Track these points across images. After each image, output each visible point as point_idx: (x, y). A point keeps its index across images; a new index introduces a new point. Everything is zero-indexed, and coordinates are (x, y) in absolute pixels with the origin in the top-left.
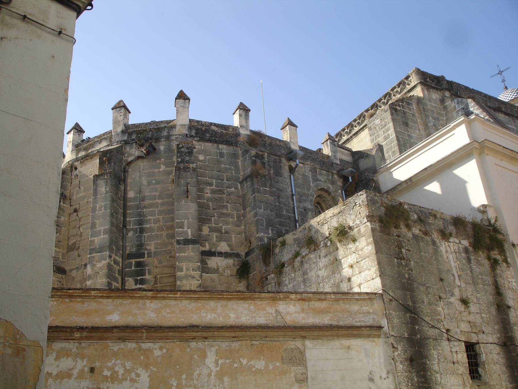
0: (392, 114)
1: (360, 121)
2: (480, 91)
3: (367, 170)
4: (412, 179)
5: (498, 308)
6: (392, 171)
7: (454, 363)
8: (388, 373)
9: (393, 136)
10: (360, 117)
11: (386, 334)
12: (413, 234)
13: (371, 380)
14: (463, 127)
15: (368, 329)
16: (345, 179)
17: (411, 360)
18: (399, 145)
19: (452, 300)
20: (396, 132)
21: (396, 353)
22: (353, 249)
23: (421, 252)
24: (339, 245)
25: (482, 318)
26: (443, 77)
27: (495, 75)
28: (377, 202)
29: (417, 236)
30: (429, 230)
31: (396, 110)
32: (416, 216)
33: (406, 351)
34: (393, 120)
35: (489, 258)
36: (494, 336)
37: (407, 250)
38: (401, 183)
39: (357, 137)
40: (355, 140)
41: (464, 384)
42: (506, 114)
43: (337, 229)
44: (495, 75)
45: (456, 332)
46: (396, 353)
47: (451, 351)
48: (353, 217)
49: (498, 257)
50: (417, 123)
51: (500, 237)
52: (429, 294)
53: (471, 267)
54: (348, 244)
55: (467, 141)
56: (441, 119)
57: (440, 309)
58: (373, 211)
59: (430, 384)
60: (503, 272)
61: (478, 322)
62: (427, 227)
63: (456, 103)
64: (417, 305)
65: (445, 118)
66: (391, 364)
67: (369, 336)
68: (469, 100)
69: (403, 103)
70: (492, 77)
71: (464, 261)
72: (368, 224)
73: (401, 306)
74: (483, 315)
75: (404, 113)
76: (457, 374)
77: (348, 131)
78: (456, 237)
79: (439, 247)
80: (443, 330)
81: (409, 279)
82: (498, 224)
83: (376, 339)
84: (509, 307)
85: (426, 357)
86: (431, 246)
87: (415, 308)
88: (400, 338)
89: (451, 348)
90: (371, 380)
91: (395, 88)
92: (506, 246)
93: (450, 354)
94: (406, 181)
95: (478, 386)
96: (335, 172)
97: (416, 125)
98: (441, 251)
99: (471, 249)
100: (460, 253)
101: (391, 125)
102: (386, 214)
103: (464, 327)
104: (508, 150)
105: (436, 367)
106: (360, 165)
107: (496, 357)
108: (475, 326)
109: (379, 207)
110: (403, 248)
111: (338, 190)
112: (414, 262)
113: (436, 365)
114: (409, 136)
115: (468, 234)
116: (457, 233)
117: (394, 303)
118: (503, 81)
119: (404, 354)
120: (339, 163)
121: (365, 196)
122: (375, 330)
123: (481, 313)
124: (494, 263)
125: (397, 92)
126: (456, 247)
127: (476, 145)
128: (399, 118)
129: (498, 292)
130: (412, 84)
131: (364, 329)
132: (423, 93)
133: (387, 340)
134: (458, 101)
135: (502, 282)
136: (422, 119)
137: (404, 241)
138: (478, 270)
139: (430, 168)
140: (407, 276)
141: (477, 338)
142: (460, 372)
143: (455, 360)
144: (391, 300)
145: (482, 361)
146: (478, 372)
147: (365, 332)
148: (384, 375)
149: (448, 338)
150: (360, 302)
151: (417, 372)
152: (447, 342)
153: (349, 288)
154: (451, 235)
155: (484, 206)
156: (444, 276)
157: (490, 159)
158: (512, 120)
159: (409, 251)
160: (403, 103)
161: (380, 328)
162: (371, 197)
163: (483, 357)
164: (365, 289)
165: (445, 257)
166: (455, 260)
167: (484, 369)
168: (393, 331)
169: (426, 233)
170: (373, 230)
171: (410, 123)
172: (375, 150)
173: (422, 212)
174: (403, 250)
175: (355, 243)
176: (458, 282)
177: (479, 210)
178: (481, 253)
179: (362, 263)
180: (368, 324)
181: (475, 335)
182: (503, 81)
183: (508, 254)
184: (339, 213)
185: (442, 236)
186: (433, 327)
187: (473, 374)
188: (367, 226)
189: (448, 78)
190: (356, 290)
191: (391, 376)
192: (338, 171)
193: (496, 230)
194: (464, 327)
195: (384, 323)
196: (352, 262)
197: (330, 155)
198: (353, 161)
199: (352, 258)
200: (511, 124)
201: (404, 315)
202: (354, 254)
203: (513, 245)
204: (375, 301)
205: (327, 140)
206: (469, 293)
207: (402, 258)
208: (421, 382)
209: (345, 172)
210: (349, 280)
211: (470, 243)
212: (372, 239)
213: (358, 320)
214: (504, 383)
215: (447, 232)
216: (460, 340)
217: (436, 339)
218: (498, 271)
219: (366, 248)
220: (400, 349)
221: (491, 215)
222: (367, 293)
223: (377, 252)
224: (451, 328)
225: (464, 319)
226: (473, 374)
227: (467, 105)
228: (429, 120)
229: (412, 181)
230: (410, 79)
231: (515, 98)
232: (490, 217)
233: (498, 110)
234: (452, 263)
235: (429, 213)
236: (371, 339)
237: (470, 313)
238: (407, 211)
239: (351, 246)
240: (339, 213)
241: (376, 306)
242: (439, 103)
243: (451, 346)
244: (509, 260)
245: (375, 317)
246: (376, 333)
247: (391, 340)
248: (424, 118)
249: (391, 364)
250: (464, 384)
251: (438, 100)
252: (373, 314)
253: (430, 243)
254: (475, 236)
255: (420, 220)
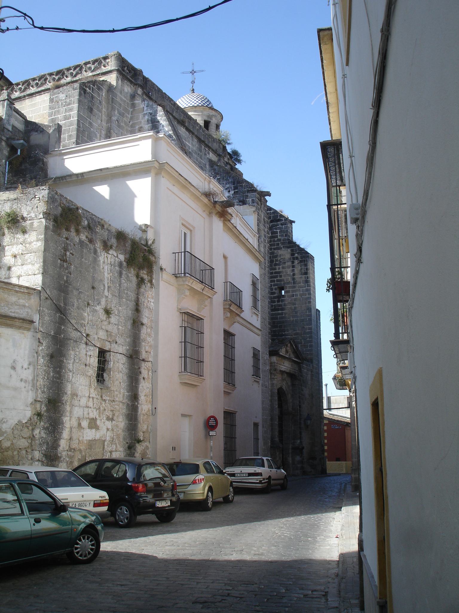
0: (80, 95)
1: (40, 83)
2: (171, 97)
3: (38, 146)
4: (84, 175)
5: (134, 323)
6: (65, 157)
7: (86, 365)
8: (30, 364)
9: (74, 119)
10: (40, 78)
11: (35, 329)
12: (80, 240)
13: (14, 368)
14: (149, 141)
15: (21, 321)
16: (13, 149)
17: (52, 356)
18: (79, 130)
19: (98, 308)
20: (79, 116)
21: (41, 348)
22: (21, 240)
23: (82, 258)
24: (6, 231)
25: (118, 329)
26: (141, 71)
27: (186, 73)
28: (56, 200)
29: (83, 242)
30: (94, 238)
31: (85, 91)
32: (86, 222)
33: (49, 347)
34: (80, 102)
35: (137, 276)
36: (124, 348)
37: (71, 253)
38: (72, 175)
39: (30, 99)
40: (27, 102)
41: (90, 385)
42: (187, 129)
43: (9, 215)
44: (186, 73)
45: (94, 338)
46: (41, 348)
47: (86, 354)
48: (29, 208)
49: (145, 277)
50: (102, 113)
51: (152, 258)
52: (80, 298)
53: (120, 281)
54: (17, 234)
55: (148, 157)
56: (126, 116)
57: (86, 314)
58: (50, 208)
59: (62, 380)
60: (146, 291)
61: (114, 332)
62: (93, 235)
63: (146, 105)
64: (67, 307)
65: (129, 116)
66: (34, 356)
67: (20, 328)
68: (160, 108)
69: (94, 86)
70: (183, 73)
71: (116, 275)
72: (43, 220)
73: (53, 305)
74: (120, 327)
75: (93, 97)
76: (87, 375)
77: (23, 88)
78: (115, 251)
79: (98, 256)
80: (84, 334)
81: (66, 282)
82: (153, 247)
83: (25, 332)
84: (142, 324)
85: (64, 356)
86: (93, 254)
87: (65, 309)
88: (46, 335)
89: (87, 351)
90: (14, 368)
91: (89, 63)
92: (155, 268)
93: (84, 356)
94: (77, 175)
95: (101, 389)
96: (4, 138)
97: (100, 114)
98: (100, 261)
99: (125, 264)
100: (115, 266)
101: (76, 106)
102: (61, 215)
103: (102, 334)
104: (182, 178)
105: (70, 367)
106: (32, 138)
107: (121, 366)
108: (111, 335)
109: (56, 207)
110: (68, 251)
111: (3, 159)
112: (75, 266)
113: (71, 364)
114: (90, 124)
115: (126, 250)
116: (117, 246)
117: (49, 302)
118: (193, 82)
119: (47, 350)
120: (10, 129)
121: (47, 192)
122: (26, 323)
123: (118, 325)
124: (141, 282)
125: (90, 68)
126: (113, 260)
127: (156, 165)
128: (86, 101)
129: (137, 310)
130: (109, 68)
131: (17, 320)
132: (117, 82)
133: (35, 334)
134: (148, 104)
135: (143, 300)
136: (107, 110)
137: (70, 244)
138: (125, 285)
139: (106, 171)
140: (65, 278)
141: (109, 347)
142: (89, 374)
143: (87, 363)
144: (47, 298)
145: (109, 367)
146: (102, 376)
147: (18, 323)
148: (26, 366)
149: (86, 342)
150: (19, 294)
151: (55, 368)
152: (84, 346)
153: (7, 276)
154: (111, 247)
155: (146, 226)
156: (96, 285)
157: (165, 182)
158: (191, 138)
159: (73, 255)
160: (94, 86)
161: (32, 322)
162: (52, 195)
163: (111, 365)
164: (24, 282)
165: (101, 267)
166: (109, 271)
167: (109, 375)
168: (42, 327)
169: (91, 241)
170: (46, 228)
171: (95, 110)
172: (53, 129)
173: (92, 219)
174: (68, 253)
175: (24, 235)
176: (106, 293)
177: (140, 228)
178: (132, 269)
179: (27, 256)
180: (22, 316)
181: (109, 343)
182: (193, 82)
183: (154, 276)
184: (15, 199)
185: (103, 246)
186: (76, 330)
187: (99, 377)
188: (41, 222)
189: (146, 74)
190: (14, 281)
191: (31, 368)
192: (8, 139)
193: (150, 252)
194: (102, 334)
195: (36, 318)
196: (17, 253)
197: (4, 117)
198: (25, 130)
199: (18, 248)
200: (189, 142)
201: (55, 314)
202: (21, 245)
203: (161, 269)
204: (32, 297)
205: (5, 100)
206: (113, 305)
207: (65, 261)
208: (55, 377)
209: (15, 142)
210: (9, 268)
211: (125, 258)
212: (43, 236)
213: (13, 311)
214: (122, 391)
215: (109, 244)
216: (95, 346)
217: (76, 341)
218: (142, 290)
219: (35, 243)
220: (44, 345)
221: (150, 236)
222: (27, 288)
223: (45, 250)
224: (91, 334)
225: (103, 327)
226: (99, 377)
227: (156, 112)
228: (115, 113)
229: (83, 176)
230: (107, 61)
231: (198, 106)
232: (148, 238)
233: (182, 123)
234: (106, 274)
235: (99, 222)
236: (21, 331)
237: (109, 323)
238: (80, 215)
239: (20, 236)
240: (15, 199)
241: (32, 300)
242: (129, 98)
243: (87, 349)
244: (154, 281)
245: (29, 311)
246: (26, 325)
247: (39, 335)
248: (110, 109)
249: (34, 356)
250: (90, 385)
251: (129, 95)
252: (28, 308)
253: (92, 251)
254: (131, 253)
255: (89, 227)
